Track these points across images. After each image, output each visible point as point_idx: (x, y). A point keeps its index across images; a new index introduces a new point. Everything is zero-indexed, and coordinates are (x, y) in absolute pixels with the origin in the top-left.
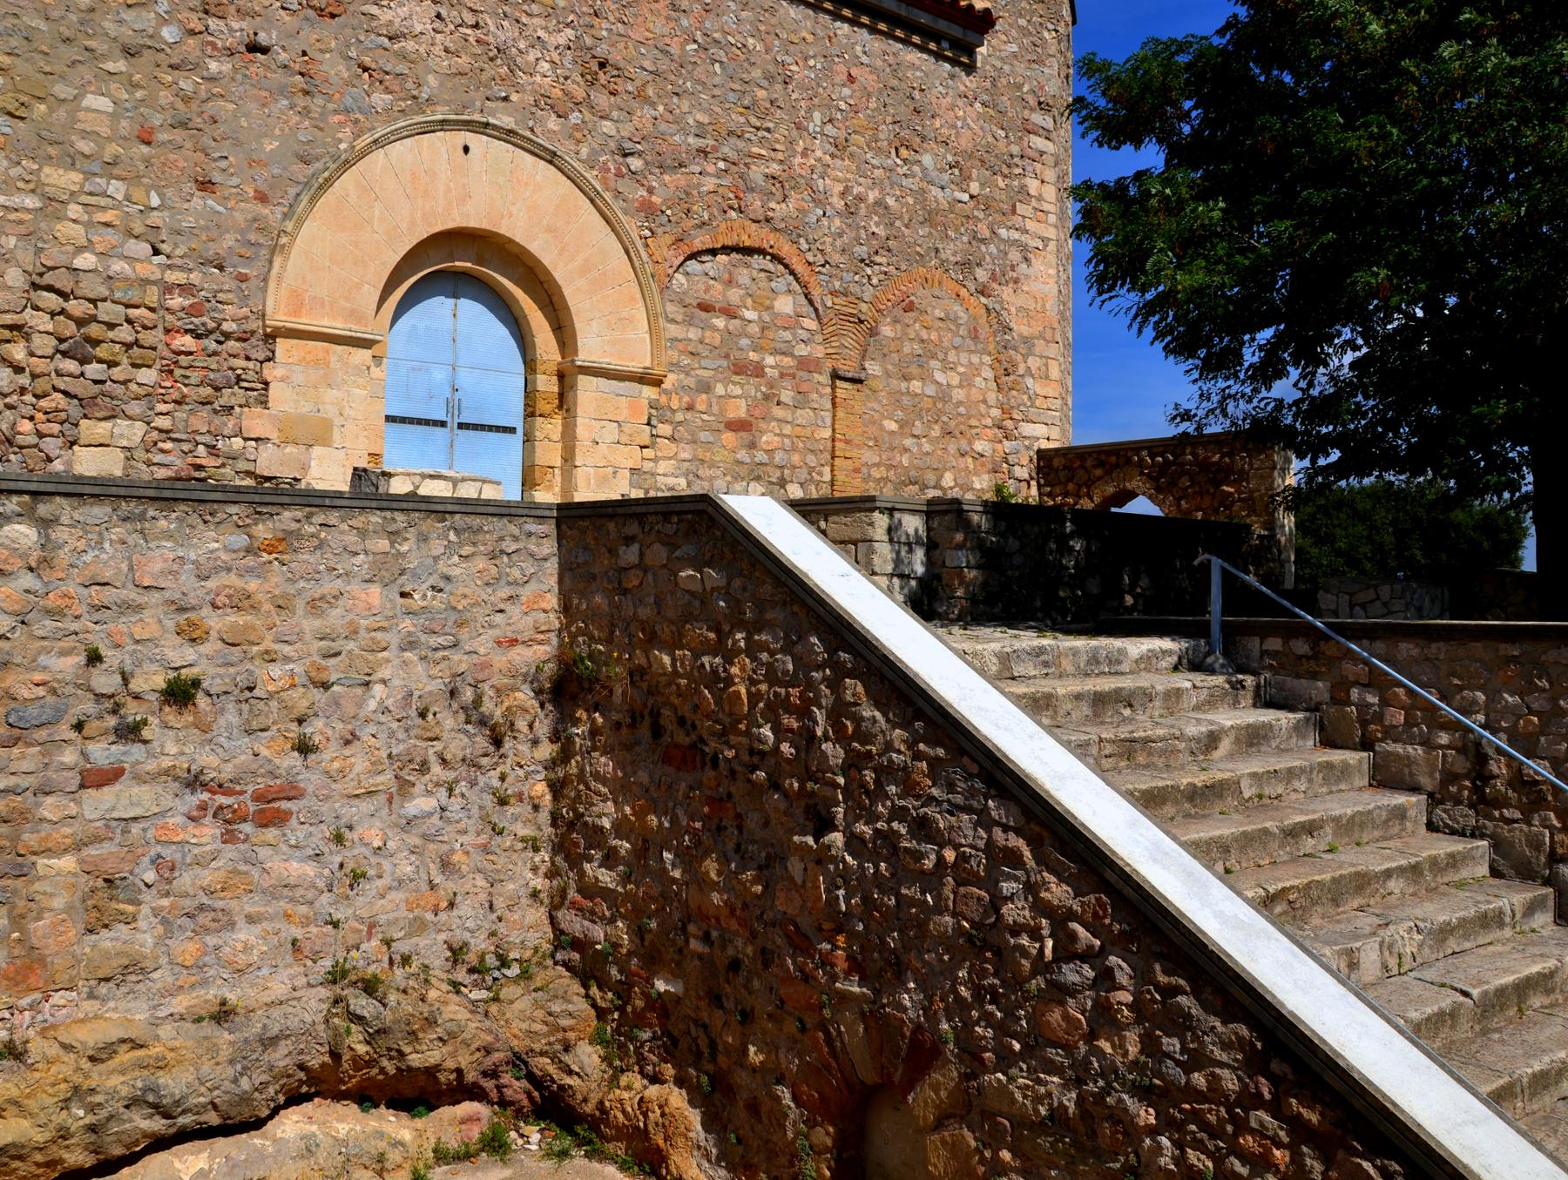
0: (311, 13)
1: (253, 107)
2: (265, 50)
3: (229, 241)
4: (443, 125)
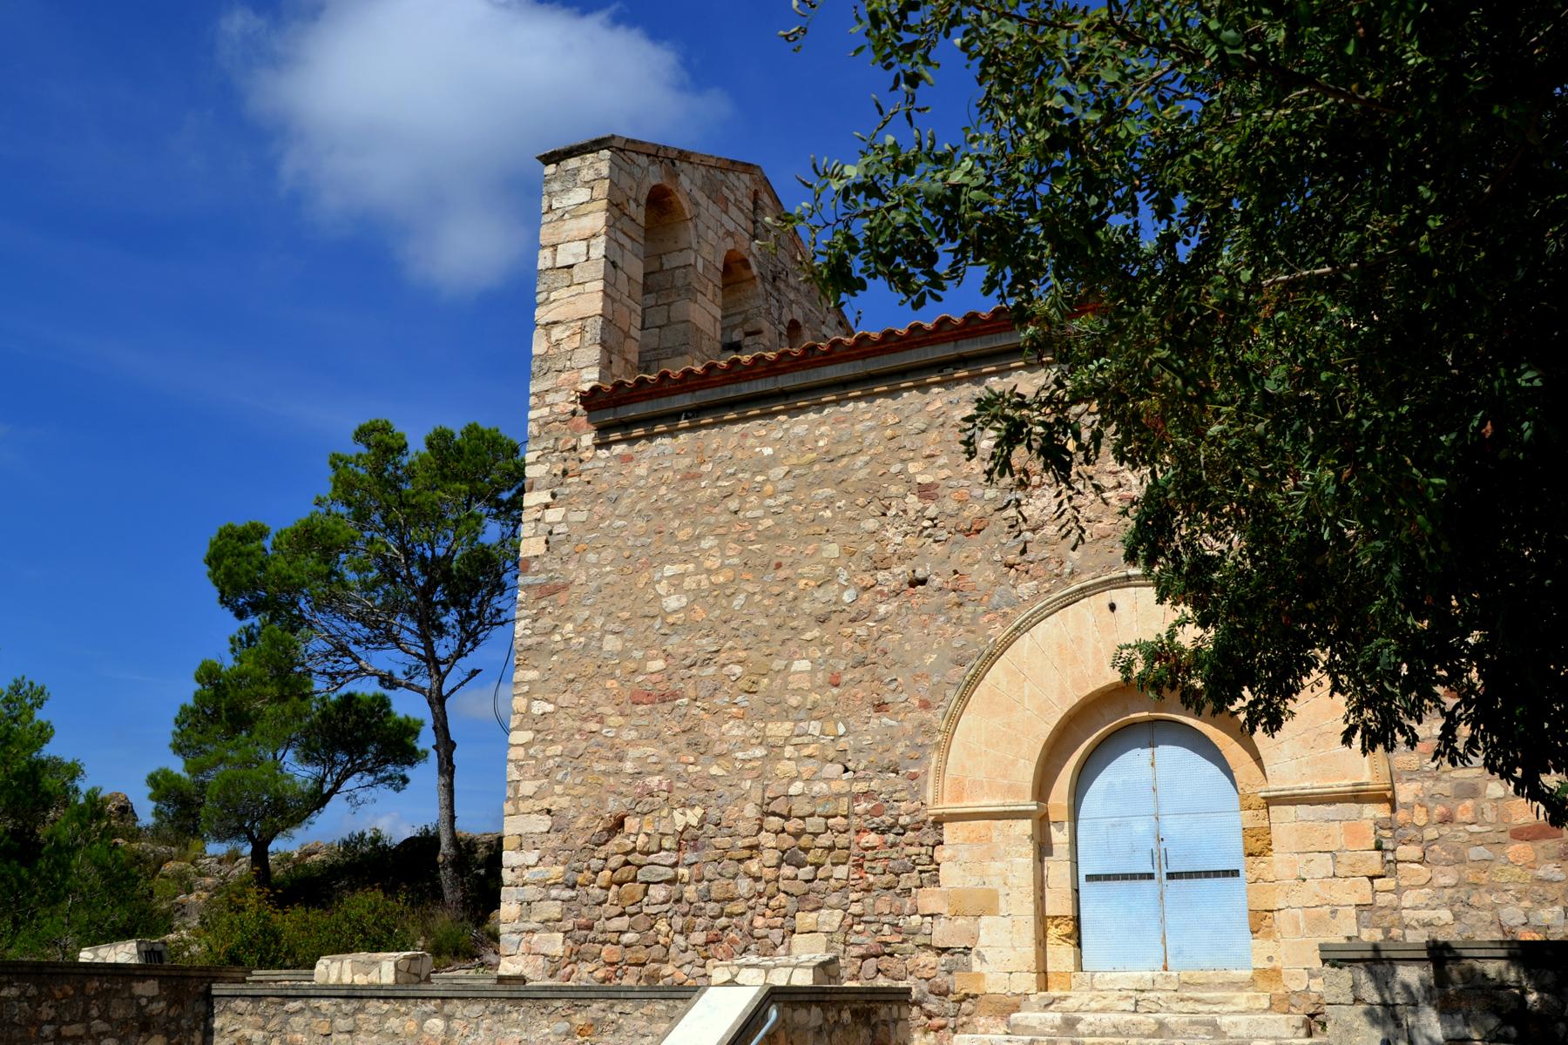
0: (959, 536)
1: (914, 632)
2: (923, 582)
3: (900, 748)
4: (1084, 592)
